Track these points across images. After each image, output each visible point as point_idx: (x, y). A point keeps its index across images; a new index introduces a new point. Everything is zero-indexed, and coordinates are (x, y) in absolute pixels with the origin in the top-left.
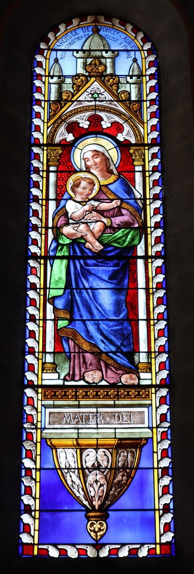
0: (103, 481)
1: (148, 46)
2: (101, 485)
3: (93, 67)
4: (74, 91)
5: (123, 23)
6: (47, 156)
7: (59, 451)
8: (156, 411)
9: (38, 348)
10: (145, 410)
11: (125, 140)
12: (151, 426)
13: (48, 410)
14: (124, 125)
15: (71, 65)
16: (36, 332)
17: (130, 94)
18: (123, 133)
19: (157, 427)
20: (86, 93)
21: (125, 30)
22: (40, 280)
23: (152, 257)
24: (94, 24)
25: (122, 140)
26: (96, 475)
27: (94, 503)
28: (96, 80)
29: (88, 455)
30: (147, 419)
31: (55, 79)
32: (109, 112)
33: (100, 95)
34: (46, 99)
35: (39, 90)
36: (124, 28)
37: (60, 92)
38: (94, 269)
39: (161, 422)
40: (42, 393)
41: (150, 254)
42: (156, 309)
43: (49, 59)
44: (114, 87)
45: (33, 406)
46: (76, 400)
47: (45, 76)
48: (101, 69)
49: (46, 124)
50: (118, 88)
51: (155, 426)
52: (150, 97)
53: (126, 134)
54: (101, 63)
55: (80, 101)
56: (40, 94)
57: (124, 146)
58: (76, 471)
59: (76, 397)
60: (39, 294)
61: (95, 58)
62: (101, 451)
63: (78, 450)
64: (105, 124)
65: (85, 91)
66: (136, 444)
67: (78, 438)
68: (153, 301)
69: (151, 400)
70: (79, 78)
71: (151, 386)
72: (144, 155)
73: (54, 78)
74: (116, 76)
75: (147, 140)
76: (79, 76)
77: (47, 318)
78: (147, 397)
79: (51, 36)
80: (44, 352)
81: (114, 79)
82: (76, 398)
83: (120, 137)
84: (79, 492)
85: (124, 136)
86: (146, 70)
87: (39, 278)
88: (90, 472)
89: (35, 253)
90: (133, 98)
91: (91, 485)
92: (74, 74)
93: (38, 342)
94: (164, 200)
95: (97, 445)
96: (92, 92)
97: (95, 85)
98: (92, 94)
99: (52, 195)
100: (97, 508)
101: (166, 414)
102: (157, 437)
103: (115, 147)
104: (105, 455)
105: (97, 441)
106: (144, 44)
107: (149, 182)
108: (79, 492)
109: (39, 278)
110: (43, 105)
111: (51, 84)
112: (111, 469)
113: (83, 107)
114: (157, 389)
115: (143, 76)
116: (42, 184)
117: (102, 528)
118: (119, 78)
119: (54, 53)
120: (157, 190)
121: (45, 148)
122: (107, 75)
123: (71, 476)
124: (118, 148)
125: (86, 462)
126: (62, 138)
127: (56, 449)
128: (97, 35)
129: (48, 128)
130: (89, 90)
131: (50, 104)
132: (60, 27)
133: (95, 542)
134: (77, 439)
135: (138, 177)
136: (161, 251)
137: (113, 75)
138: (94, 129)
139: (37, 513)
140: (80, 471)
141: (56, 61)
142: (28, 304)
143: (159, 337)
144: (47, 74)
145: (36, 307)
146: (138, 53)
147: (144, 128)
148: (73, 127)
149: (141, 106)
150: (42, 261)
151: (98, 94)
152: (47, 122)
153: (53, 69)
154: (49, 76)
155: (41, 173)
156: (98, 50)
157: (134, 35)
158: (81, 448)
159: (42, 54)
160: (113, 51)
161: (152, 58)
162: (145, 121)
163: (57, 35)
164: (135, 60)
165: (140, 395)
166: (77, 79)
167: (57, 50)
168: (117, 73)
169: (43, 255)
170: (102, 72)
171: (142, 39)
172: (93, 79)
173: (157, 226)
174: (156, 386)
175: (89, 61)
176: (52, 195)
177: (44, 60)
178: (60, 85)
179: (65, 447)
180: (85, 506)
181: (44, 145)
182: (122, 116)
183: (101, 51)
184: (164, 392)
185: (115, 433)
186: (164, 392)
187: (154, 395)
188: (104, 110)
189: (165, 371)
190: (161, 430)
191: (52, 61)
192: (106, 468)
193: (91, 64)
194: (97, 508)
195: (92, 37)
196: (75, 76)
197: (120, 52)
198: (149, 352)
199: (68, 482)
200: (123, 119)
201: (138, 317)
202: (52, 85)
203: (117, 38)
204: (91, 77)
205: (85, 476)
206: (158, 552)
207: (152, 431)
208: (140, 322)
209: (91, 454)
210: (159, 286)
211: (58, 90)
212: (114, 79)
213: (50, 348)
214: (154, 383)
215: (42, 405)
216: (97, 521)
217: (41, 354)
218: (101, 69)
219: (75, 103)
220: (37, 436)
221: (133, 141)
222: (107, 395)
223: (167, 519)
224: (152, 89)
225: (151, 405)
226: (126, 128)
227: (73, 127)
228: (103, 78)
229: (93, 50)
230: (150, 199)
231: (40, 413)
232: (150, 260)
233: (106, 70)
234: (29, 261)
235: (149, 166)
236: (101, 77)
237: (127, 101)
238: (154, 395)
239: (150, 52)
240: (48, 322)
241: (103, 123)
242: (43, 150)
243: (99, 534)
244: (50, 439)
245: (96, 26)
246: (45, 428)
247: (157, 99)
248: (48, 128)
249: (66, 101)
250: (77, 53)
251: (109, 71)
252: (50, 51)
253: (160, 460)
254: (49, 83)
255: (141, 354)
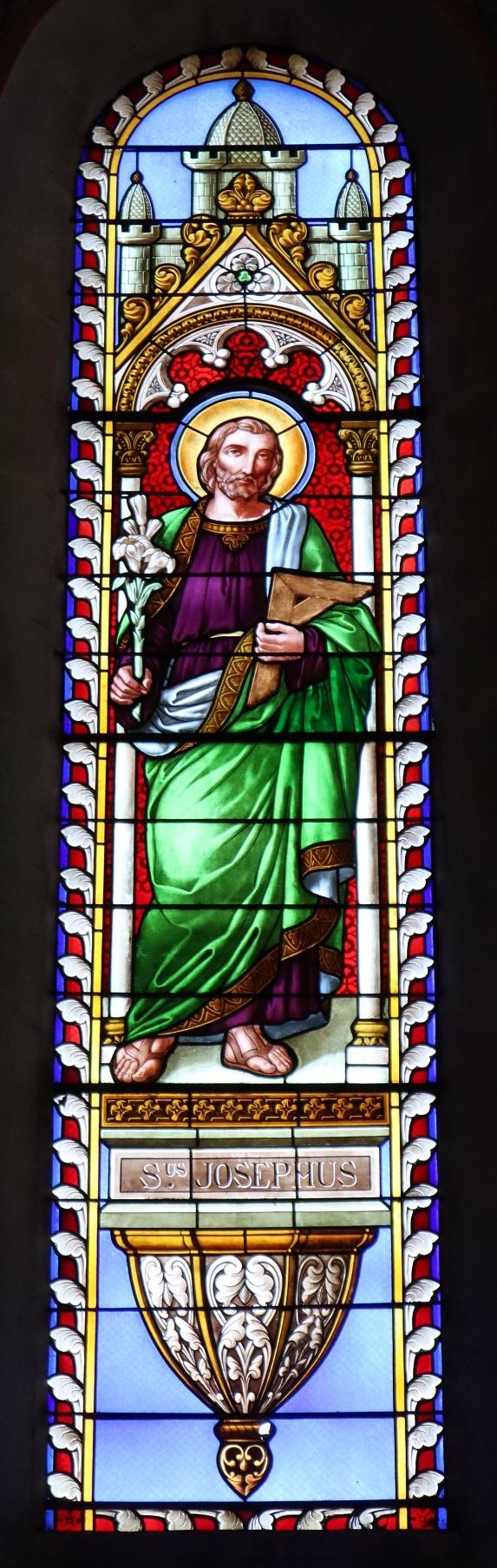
0: (258, 1340)
1: (389, 134)
2: (257, 1351)
3: (238, 196)
4: (187, 264)
5: (319, 70)
6: (115, 448)
7: (145, 1261)
8: (406, 1392)
9: (89, 979)
10: (373, 1151)
11: (328, 401)
12: (386, 1194)
13: (117, 1153)
14: (324, 357)
15: (175, 191)
16: (81, 1122)
17: (337, 270)
18: (323, 383)
19: (403, 1198)
20: (218, 271)
21: (326, 90)
22: (96, 798)
23: (394, 737)
24: (238, 74)
25: (319, 400)
26: (245, 1324)
27: (238, 1397)
28: (244, 234)
29: (222, 1272)
30: (381, 1177)
31: (134, 232)
32: (280, 322)
33: (258, 276)
34: (92, 1305)
35: (91, 260)
36: (320, 84)
37: (149, 267)
38: (236, 755)
39: (414, 1183)
40: (99, 1108)
41: (389, 728)
42: (408, 1150)
43: (117, 175)
44: (297, 252)
45: (80, 1046)
46: (190, 1127)
47: (108, 222)
48: (259, 201)
49: (110, 358)
50: (308, 254)
51: (397, 1194)
52: (394, 281)
53: (332, 385)
54: (258, 185)
55: (202, 294)
56: (87, 541)
57: (322, 420)
58: (191, 1313)
59: (189, 1118)
60: (94, 835)
61: (242, 171)
62: (252, 1263)
63: (196, 1260)
64: (273, 357)
65: (217, 264)
66: (347, 1243)
67: (198, 1228)
68: (398, 945)
69: (389, 1126)
70: (200, 228)
71: (389, 1087)
72: (378, 446)
73: (132, 227)
74: (299, 220)
75: (385, 402)
76: (200, 222)
77: (115, 902)
78: (380, 1116)
79: (121, 107)
80: (106, 992)
81: (294, 230)
82: (189, 1122)
83: (313, 394)
84: (196, 1368)
85: (323, 391)
86: (382, 204)
87: (95, 793)
88: (227, 1317)
89: (83, 723)
90: (349, 283)
91: (232, 1352)
92: (186, 216)
93: (98, 626)
94: (439, 1000)
95: (245, 1247)
96: (235, 268)
97: (243, 248)
98: (237, 274)
99: (124, 808)
100: (245, 1410)
101: (408, 321)
102: (402, 1217)
103: (298, 423)
104: (266, 1272)
105: (245, 1235)
106: (376, 128)
107: (398, 945)
108: (196, 1368)
109: (93, 878)
110: (103, 234)
111: (122, 245)
112: (280, 1308)
113: (212, 310)
114: (404, 1095)
115: (373, 220)
116: (106, 262)
117: (257, 1463)
118: (308, 227)
119: (130, 157)
120: (413, 624)
121: (95, 1097)
122: (276, 219)
123: (177, 1328)
124: (304, 425)
125: (215, 1290)
126: (151, 398)
127: (138, 1258)
128: (245, 105)
129: (115, 371)
130: (227, 262)
131: (121, 304)
132: (146, 82)
133: (235, 1498)
134: (193, 1232)
135: (361, 511)
136: (432, 1401)
137: (290, 219)
138: (240, 372)
139: (105, 659)
140: (202, 1314)
141: (137, 178)
142: (58, 1133)
143: (406, 784)
144: (113, 216)
145: (89, 701)
146: (359, 155)
147: (376, 370)
148: (183, 365)
149: (369, 303)
150: (103, 749)
151: (252, 274)
152: (115, 355)
153: (127, 202)
154: (118, 221)
155: (98, 498)
156: (251, 148)
157: (350, 105)
158: (200, 1252)
159: (100, 163)
160: (293, 150)
161: (399, 169)
162: (381, 347)
163: (139, 106)
164: (352, 176)
165: (359, 1112)
166: (195, 231)
167: (139, 149)
168: (303, 214)
169: (109, 408)
170: (263, 212)
171: (371, 115)
172: (238, 230)
173: (410, 645)
174: (399, 1087)
175: (227, 177)
176: (124, 808)
177: (100, 437)
178: (149, 247)
179: (161, 1251)
180: (212, 1405)
181: (105, 416)
182: (319, 333)
183: (260, 149)
184: (422, 1104)
185: (294, 1212)
186: (422, 1104)
187: (395, 1112)
188: (271, 320)
189: (426, 1048)
190: (413, 1205)
191: (125, 182)
192: (269, 1306)
193: (231, 186)
194: (245, 1410)
195: (233, 109)
196: (190, 220)
197: (310, 153)
198: (384, 994)
199: (170, 1344)
200: (320, 341)
201: (351, 562)
202: (125, 249)
203: (301, 114)
204: (232, 222)
205: (215, 1331)
206: (403, 1523)
207: (390, 1208)
208: (355, 501)
209: (229, 1270)
210: (409, 567)
211: (143, 266)
212: (294, 230)
213: (119, 982)
214: (395, 1080)
215: (101, 1141)
216: (244, 1446)
217: (97, 999)
218: (259, 201)
219: (190, 298)
220: (88, 1220)
221: (347, 401)
222: (272, 1112)
223: (417, 926)
224: (399, 258)
225: (389, 1138)
226: (331, 368)
227: (183, 365)
228: (264, 229)
229: (236, 148)
230: (396, 820)
231: (97, 1163)
232: (389, 748)
233: (271, 205)
234: (74, 427)
235: (398, 893)
236: (258, 222)
237: (333, 295)
238: (395, 1112)
239: (392, 152)
240: (118, 826)
241: (265, 353)
242: (102, 430)
243: (249, 1478)
244: (123, 1230)
245: (243, 79)
246: (109, 1201)
247: (410, 214)
248: (115, 371)
249: (165, 293)
250: (194, 156)
251: (282, 206)
252: (118, 152)
253: (412, 1333)
254: (117, 243)
255: (362, 1000)
